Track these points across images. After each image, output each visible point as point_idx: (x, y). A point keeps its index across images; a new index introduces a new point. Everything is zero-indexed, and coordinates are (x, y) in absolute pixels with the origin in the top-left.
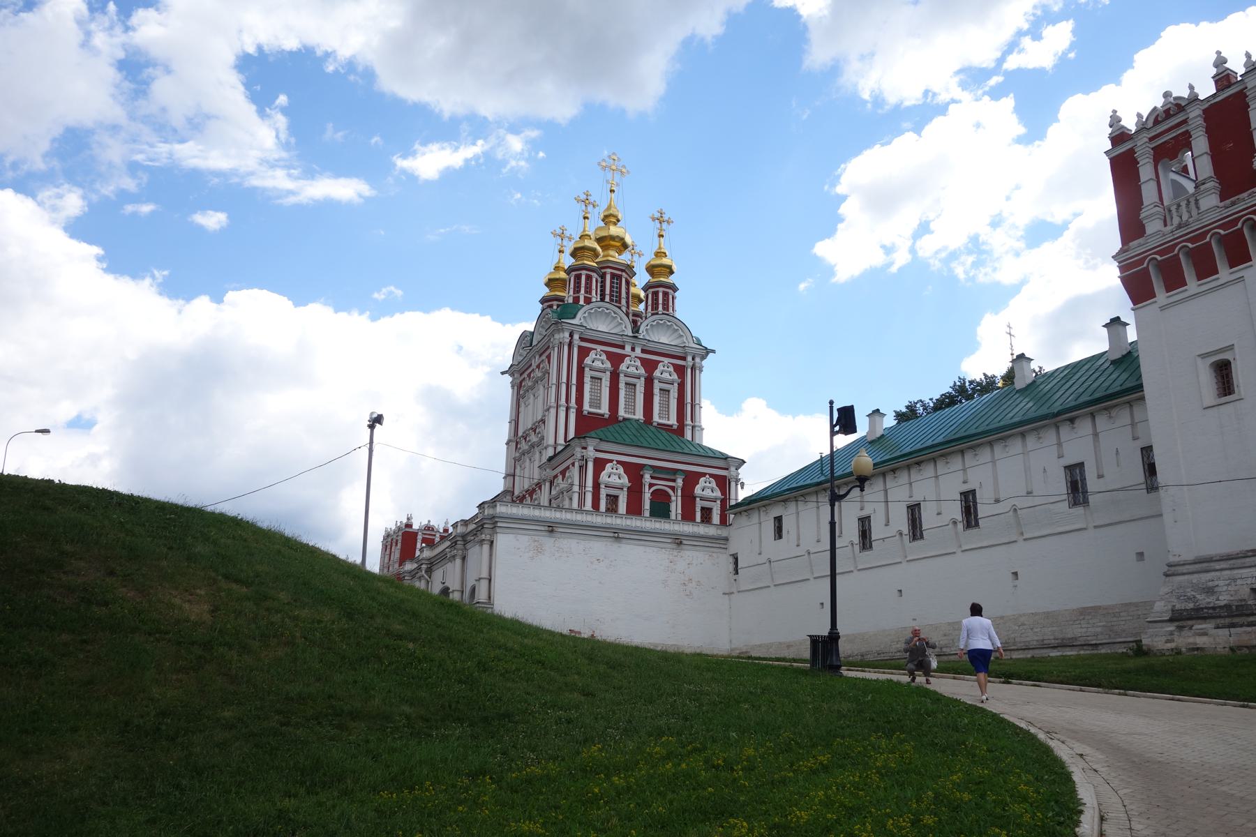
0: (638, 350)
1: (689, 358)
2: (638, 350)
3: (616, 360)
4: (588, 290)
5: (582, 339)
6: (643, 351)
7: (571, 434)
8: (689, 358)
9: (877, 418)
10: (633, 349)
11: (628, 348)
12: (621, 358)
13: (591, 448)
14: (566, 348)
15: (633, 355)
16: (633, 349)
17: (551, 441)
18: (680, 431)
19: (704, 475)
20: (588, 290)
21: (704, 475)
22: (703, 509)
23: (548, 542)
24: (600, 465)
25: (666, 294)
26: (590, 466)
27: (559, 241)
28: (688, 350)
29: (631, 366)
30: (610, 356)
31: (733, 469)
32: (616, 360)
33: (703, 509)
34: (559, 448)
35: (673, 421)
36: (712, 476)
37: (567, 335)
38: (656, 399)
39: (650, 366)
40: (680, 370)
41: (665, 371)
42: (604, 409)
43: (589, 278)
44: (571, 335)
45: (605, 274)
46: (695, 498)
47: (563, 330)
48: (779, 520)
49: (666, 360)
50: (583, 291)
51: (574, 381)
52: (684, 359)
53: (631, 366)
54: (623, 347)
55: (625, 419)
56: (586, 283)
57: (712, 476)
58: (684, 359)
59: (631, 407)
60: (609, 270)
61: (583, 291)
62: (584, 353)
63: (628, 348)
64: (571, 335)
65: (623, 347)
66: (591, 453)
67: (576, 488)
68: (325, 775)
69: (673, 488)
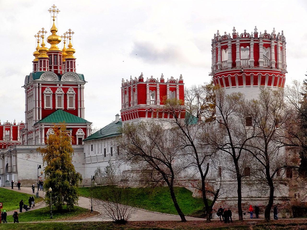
0: (61, 85)
1: (79, 86)
2: (61, 85)
3: (54, 90)
4: (44, 66)
5: (42, 85)
6: (63, 85)
7: (41, 119)
8: (79, 86)
9: (117, 117)
10: (60, 85)
11: (58, 85)
12: (56, 89)
13: (43, 125)
14: (37, 89)
15: (60, 87)
16: (60, 85)
17: (34, 119)
18: (75, 112)
19: (79, 128)
20: (44, 66)
21: (79, 128)
22: (79, 138)
23: (31, 155)
24: (46, 130)
25: (71, 62)
26: (43, 130)
27: (37, 38)
28: (78, 83)
29: (60, 91)
30: (52, 89)
31: (88, 126)
32: (54, 90)
33: (79, 138)
34: (37, 121)
35: (74, 108)
36: (81, 128)
37: (37, 84)
38: (68, 101)
39: (65, 90)
40: (76, 90)
41: (71, 91)
42: (51, 107)
43: (44, 61)
44: (39, 84)
45: (51, 55)
46: (76, 136)
47: (36, 83)
48: (92, 145)
49: (71, 87)
50: (70, 67)
51: (41, 99)
52: (77, 85)
53: (60, 91)
54: (56, 85)
55: (58, 109)
56: (44, 63)
57: (81, 128)
58: (77, 85)
59: (60, 105)
60: (53, 54)
61: (70, 67)
62: (43, 89)
63: (58, 85)
64: (39, 84)
65: (56, 85)
66: (43, 127)
67: (40, 137)
68: (163, 201)
69: (69, 134)
